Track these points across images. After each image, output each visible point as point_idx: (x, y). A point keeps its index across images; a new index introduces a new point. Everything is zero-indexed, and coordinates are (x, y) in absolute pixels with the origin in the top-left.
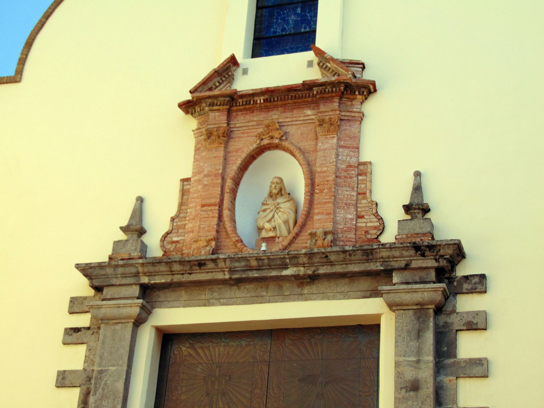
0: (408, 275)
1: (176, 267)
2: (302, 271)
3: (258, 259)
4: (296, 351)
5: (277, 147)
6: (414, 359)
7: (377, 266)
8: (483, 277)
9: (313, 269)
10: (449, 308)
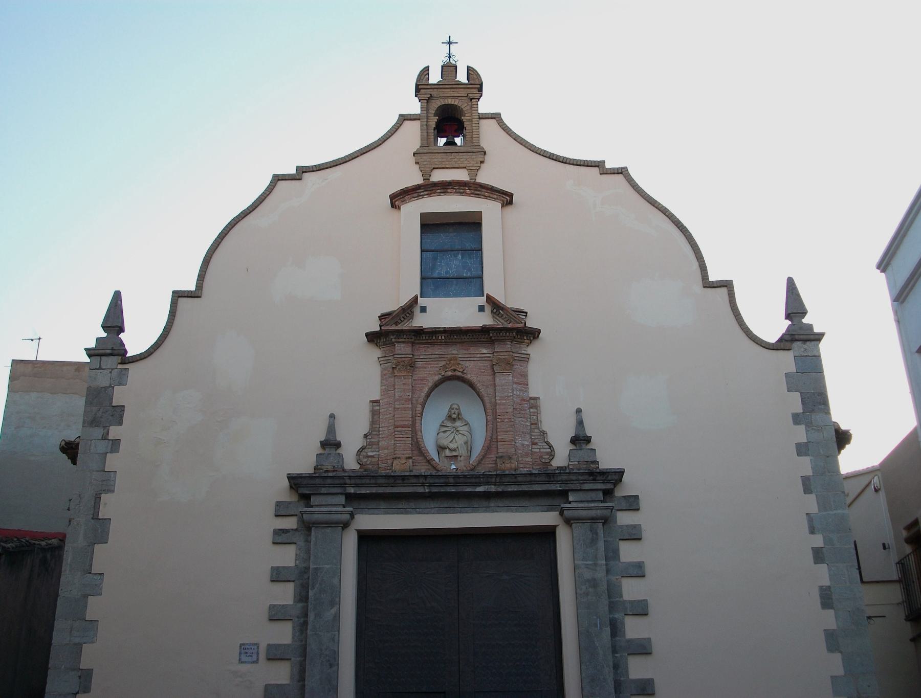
7: (558, 487)
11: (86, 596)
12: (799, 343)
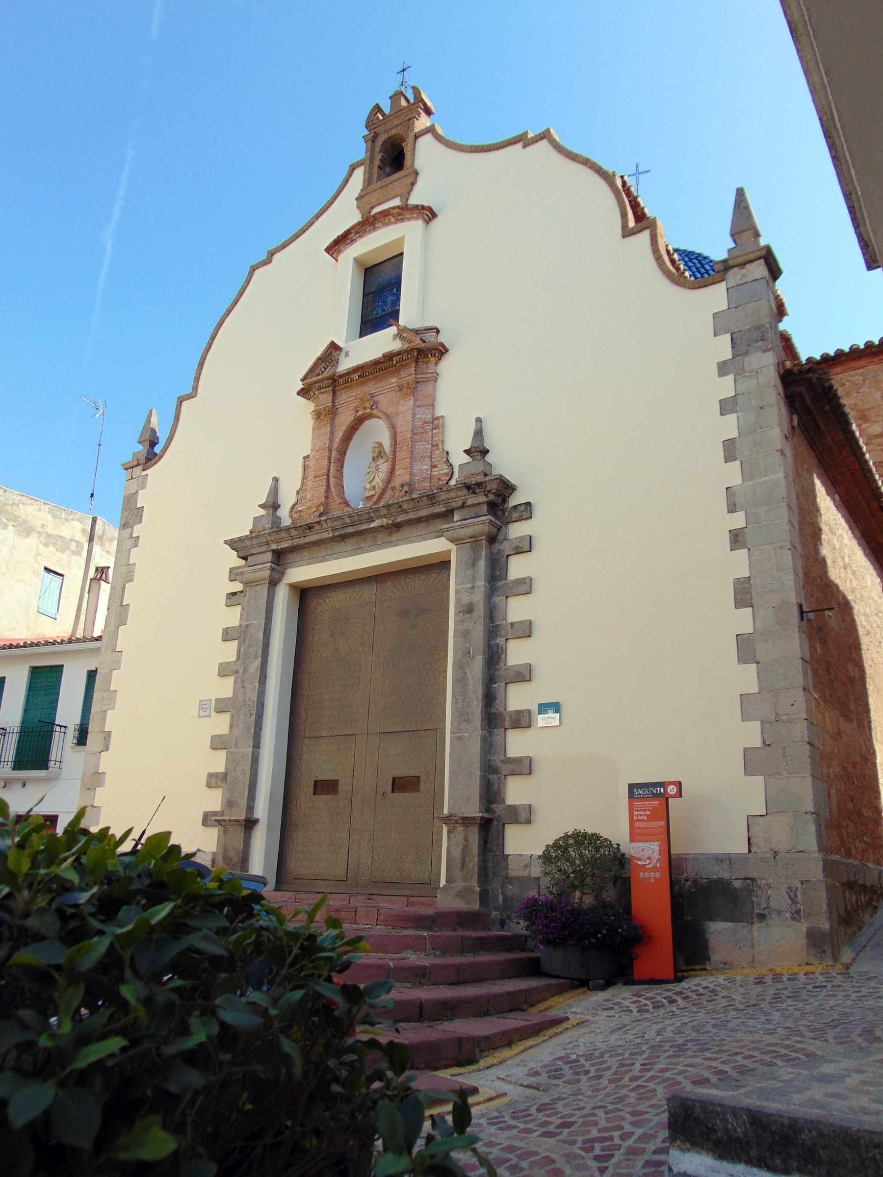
0: (465, 512)
1: (294, 533)
2: (384, 521)
3: (350, 517)
4: (395, 591)
5: (371, 416)
6: (470, 585)
7: (441, 509)
8: (528, 504)
9: (393, 518)
10: (501, 537)
11: (111, 671)
12: (735, 270)
